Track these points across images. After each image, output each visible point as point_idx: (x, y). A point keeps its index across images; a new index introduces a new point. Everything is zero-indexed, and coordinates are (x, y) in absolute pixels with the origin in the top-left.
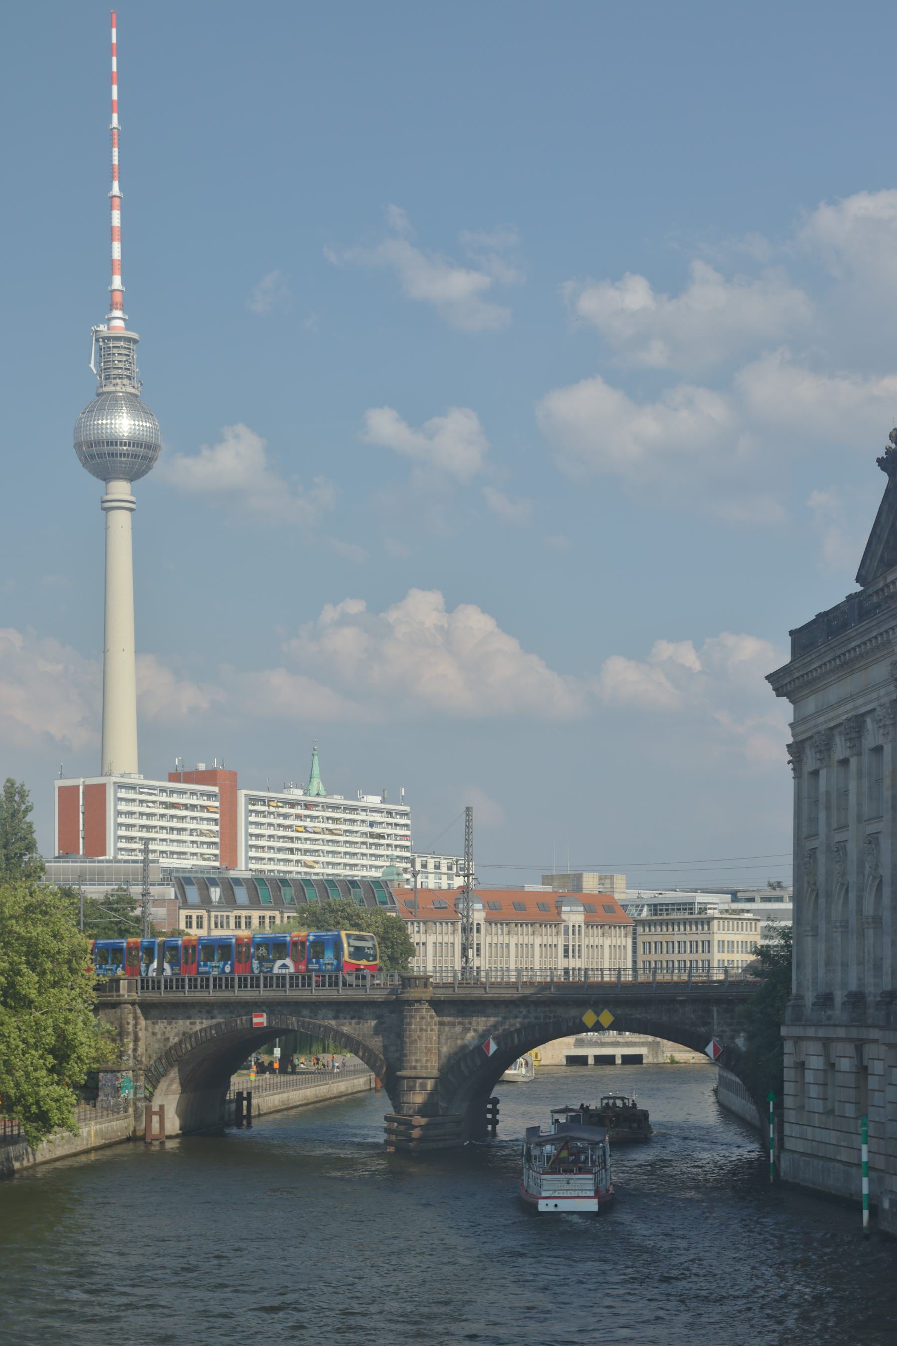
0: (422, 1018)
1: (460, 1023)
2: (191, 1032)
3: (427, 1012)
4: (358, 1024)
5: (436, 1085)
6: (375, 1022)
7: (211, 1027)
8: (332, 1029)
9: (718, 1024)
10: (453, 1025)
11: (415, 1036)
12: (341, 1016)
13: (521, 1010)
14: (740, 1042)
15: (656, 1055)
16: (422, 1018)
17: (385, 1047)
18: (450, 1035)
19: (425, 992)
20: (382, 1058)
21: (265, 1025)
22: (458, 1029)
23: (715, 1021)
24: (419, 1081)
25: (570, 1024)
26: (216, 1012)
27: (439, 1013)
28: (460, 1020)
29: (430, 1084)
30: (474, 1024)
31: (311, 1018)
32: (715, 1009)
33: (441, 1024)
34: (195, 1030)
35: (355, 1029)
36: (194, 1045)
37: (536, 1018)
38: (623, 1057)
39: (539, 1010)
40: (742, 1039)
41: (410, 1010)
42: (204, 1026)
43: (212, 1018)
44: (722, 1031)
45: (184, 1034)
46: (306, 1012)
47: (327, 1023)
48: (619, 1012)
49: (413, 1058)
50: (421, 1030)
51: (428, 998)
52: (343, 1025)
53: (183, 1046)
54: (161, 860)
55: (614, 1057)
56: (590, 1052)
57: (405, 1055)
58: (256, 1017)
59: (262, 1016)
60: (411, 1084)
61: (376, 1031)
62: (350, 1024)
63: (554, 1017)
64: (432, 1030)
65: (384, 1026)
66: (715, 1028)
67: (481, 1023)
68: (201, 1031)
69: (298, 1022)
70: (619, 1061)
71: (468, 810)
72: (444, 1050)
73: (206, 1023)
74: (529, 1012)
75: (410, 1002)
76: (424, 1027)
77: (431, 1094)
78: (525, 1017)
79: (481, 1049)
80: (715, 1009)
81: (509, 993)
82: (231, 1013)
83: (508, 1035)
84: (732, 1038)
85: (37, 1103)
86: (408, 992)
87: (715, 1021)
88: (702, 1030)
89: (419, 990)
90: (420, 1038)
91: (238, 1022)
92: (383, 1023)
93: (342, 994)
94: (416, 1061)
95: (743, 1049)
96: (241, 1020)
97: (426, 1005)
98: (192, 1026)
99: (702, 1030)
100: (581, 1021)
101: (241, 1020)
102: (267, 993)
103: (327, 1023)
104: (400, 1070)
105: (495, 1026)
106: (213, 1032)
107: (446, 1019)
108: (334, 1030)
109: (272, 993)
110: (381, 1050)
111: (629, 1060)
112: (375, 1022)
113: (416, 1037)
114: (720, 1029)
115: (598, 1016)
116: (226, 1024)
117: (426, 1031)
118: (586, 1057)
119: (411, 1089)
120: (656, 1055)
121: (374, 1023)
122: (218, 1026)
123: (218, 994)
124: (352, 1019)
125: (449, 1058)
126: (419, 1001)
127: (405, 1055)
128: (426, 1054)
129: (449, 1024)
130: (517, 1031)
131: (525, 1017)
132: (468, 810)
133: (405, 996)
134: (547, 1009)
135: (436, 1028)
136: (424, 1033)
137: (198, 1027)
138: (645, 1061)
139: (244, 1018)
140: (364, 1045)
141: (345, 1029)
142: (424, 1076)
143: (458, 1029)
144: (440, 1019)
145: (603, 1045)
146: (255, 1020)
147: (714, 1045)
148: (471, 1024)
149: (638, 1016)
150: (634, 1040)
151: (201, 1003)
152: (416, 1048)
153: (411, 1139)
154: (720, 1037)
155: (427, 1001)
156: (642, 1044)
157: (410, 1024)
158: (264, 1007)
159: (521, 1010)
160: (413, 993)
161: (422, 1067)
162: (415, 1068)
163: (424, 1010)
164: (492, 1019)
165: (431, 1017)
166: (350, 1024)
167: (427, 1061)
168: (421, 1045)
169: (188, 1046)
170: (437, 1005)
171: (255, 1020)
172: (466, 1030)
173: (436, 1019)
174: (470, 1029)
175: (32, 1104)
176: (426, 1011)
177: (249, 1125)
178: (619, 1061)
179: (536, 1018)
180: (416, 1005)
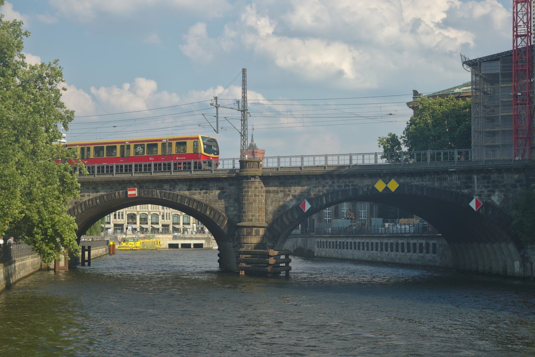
1: (281, 191)
2: (81, 202)
3: (259, 184)
4: (206, 193)
5: (265, 232)
6: (219, 191)
7: (96, 198)
8: (186, 197)
9: (478, 187)
10: (277, 192)
13: (327, 181)
16: (256, 188)
17: (226, 208)
18: (274, 199)
19: (257, 171)
20: (224, 215)
21: (137, 195)
22: (281, 195)
23: (476, 185)
24: (254, 229)
25: (365, 190)
27: (266, 184)
28: (282, 189)
29: (262, 231)
30: (292, 191)
31: (170, 190)
32: (475, 177)
33: (268, 192)
34: (84, 200)
35: (203, 197)
36: (84, 210)
37: (339, 186)
38: (182, 244)
39: (341, 181)
40: (497, 197)
41: (248, 183)
42: (91, 197)
43: (97, 192)
44: (481, 192)
46: (166, 186)
47: (182, 192)
48: (402, 181)
49: (250, 214)
50: (255, 195)
51: (260, 175)
52: (194, 194)
53: (76, 211)
55: (178, 245)
56: (180, 242)
57: (244, 212)
58: (130, 190)
59: (135, 190)
60: (249, 231)
61: (220, 197)
62: (200, 193)
64: (262, 196)
65: (225, 194)
66: (476, 190)
67: (297, 190)
68: (89, 200)
69: (161, 193)
70: (180, 246)
71: (244, 71)
72: (270, 209)
73: (93, 195)
74: (333, 183)
75: (247, 177)
78: (330, 186)
79: (298, 208)
80: (475, 177)
81: (320, 171)
83: (318, 197)
84: (489, 196)
86: (246, 171)
87: (476, 185)
88: (466, 191)
89: (254, 169)
90: (254, 201)
91: (117, 194)
92: (225, 192)
93: (195, 174)
94: (252, 216)
95: (498, 203)
96: (119, 193)
97: (258, 180)
98: (82, 198)
99: (466, 191)
100: (373, 187)
101: (119, 193)
102: (137, 175)
103: (182, 192)
104: (239, 222)
105: (308, 192)
106: (98, 201)
108: (188, 198)
111: (196, 246)
112: (219, 191)
113: (252, 201)
114: (480, 190)
115: (387, 184)
116: (107, 195)
117: (259, 196)
119: (249, 234)
121: (218, 192)
122: (101, 197)
123: (101, 176)
124: (201, 190)
125: (275, 213)
126: (254, 177)
127: (244, 212)
128: (259, 211)
129: (274, 192)
130: (324, 194)
131: (330, 186)
132: (244, 71)
133: (245, 173)
134: (347, 180)
135: (264, 194)
137: (86, 198)
139: (121, 191)
141: (197, 197)
142: (258, 225)
143: (281, 195)
144: (267, 189)
145: (185, 239)
148: (290, 191)
149: (416, 183)
151: (89, 182)
152: (252, 207)
153: (269, 265)
154: (480, 195)
155: (260, 176)
156: (203, 239)
157: (248, 191)
158: (135, 184)
160: (249, 171)
162: (251, 220)
164: (306, 188)
165: (262, 187)
166: (200, 193)
167: (259, 216)
168: (255, 205)
172: (286, 195)
173: (264, 189)
174: (289, 195)
176: (258, 184)
177: (89, 265)
178: (180, 246)
179: (339, 186)
180: (252, 179)
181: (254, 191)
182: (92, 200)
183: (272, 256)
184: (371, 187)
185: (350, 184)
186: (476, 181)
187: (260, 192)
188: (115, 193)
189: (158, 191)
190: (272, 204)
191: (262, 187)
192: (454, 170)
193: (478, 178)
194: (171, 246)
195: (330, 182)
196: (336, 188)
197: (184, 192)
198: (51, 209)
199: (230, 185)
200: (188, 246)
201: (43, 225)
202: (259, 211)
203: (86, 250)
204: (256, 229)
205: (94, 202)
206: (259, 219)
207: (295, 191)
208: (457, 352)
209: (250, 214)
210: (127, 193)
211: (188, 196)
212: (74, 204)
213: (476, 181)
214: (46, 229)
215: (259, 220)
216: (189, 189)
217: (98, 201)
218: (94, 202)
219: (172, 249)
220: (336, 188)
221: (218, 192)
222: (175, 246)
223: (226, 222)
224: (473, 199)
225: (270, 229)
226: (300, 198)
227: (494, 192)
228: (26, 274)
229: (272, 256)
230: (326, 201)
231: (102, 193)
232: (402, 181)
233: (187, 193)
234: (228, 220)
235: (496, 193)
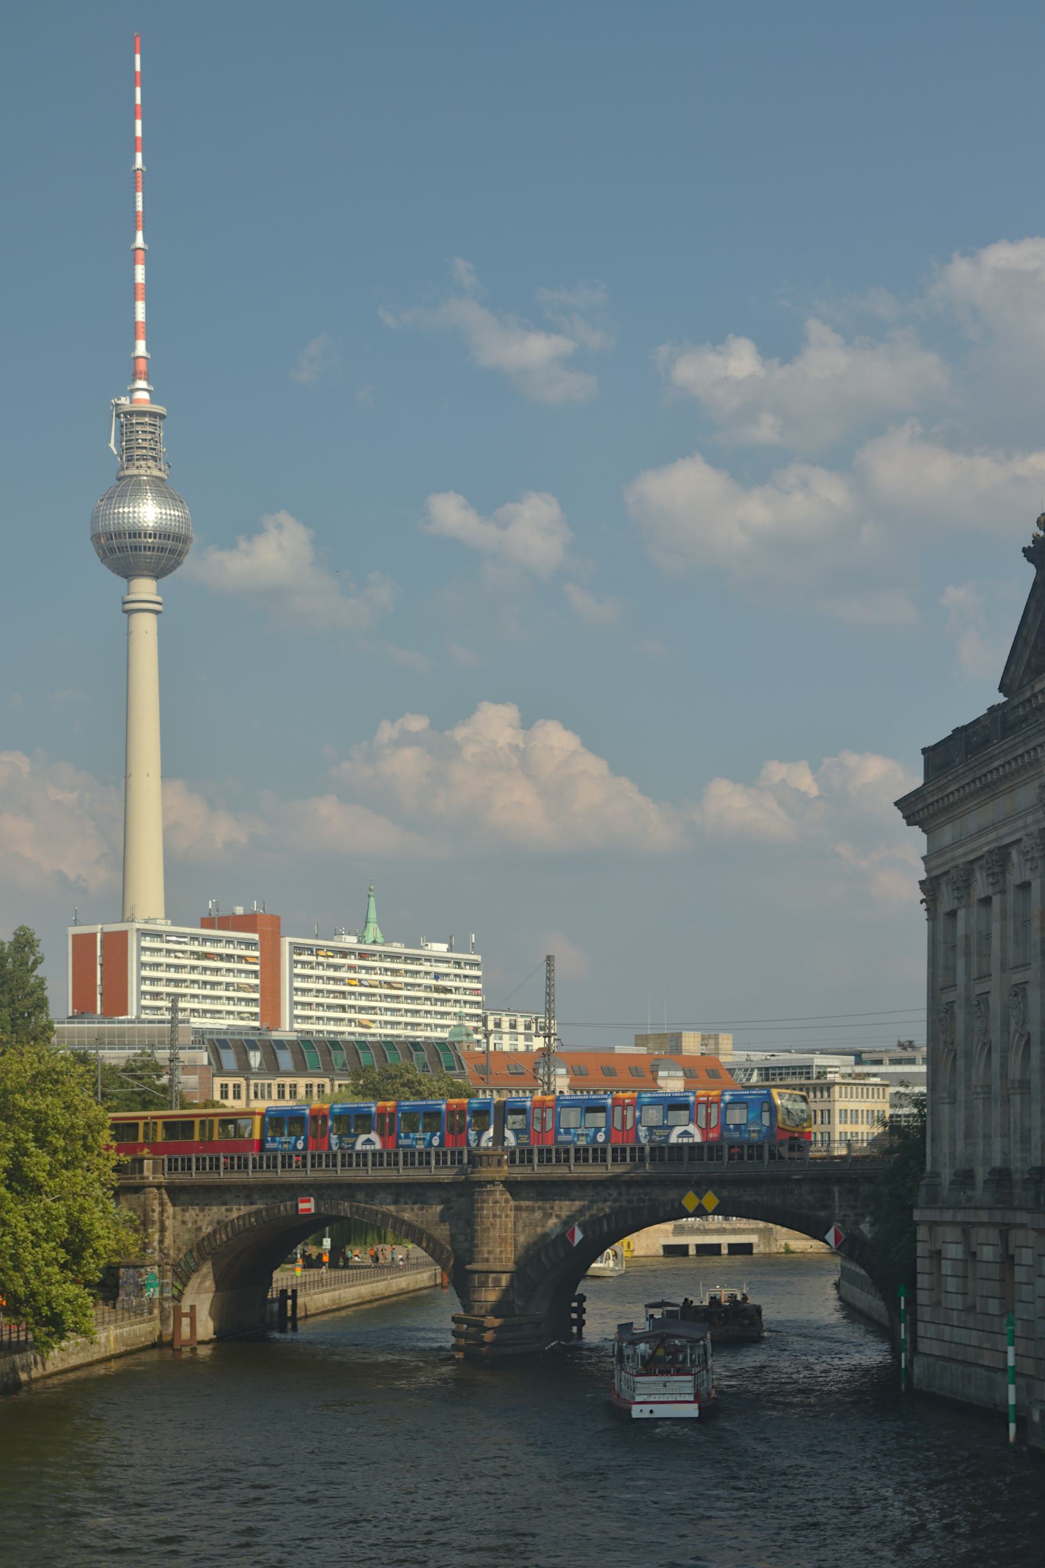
0: (496, 1202)
1: (539, 1208)
2: (227, 1220)
3: (502, 1194)
4: (422, 1209)
5: (512, 1280)
7: (250, 1215)
9: (841, 1206)
10: (532, 1210)
16: (496, 1202)
17: (453, 1237)
20: (450, 1249)
21: (313, 1211)
22: (538, 1215)
23: (837, 1204)
25: (669, 1208)
26: (256, 1196)
27: (515, 1196)
28: (540, 1204)
29: (505, 1279)
30: (556, 1208)
31: (366, 1203)
32: (836, 1189)
33: (518, 1209)
34: (231, 1218)
35: (417, 1216)
36: (230, 1235)
37: (628, 1201)
39: (632, 1192)
41: (481, 1193)
43: (252, 1204)
44: (844, 1215)
46: (360, 1196)
47: (384, 1208)
48: (725, 1193)
49: (485, 1249)
50: (495, 1216)
52: (404, 1211)
53: (218, 1236)
54: (192, 1020)
55: (719, 1246)
56: (692, 1241)
57: (476, 1246)
58: (302, 1201)
59: (309, 1201)
60: (483, 1279)
61: (443, 1218)
62: (412, 1210)
63: (649, 1200)
64: (507, 1216)
67: (565, 1208)
68: (238, 1218)
69: (351, 1207)
71: (549, 959)
72: (522, 1239)
73: (244, 1210)
74: (620, 1194)
75: (481, 1184)
76: (498, 1213)
78: (615, 1201)
79: (564, 1237)
80: (836, 1189)
83: (596, 1221)
84: (857, 1223)
86: (479, 1172)
87: (837, 1204)
90: (493, 1225)
91: (282, 1209)
94: (489, 1252)
96: (285, 1206)
97: (501, 1187)
98: (228, 1214)
99: (822, 1214)
100: (680, 1204)
101: (285, 1206)
104: (470, 1263)
106: (253, 1220)
107: (524, 1204)
108: (393, 1217)
110: (448, 1239)
113: (488, 1225)
114: (842, 1213)
115: (701, 1198)
116: (267, 1210)
117: (500, 1217)
119: (483, 1284)
122: (258, 1212)
123: (259, 1175)
124: (414, 1204)
125: (527, 1248)
126: (492, 1182)
127: (476, 1246)
128: (501, 1243)
129: (527, 1208)
130: (607, 1216)
131: (615, 1201)
132: (549, 959)
133: (476, 1177)
135: (512, 1214)
136: (498, 1220)
137: (235, 1215)
138: (755, 1251)
141: (407, 1216)
142: (498, 1269)
143: (538, 1215)
145: (706, 1232)
146: (301, 1206)
147: (836, 1231)
148: (552, 1208)
149: (747, 1198)
150: (742, 1226)
153: (483, 1344)
154: (843, 1222)
155: (502, 1182)
156: (752, 1231)
157: (482, 1209)
162: (487, 1260)
163: (498, 1193)
165: (507, 1201)
166: (412, 1210)
167: (501, 1252)
168: (494, 1233)
169: (223, 1236)
170: (513, 1187)
171: (301, 1206)
172: (547, 1216)
173: (512, 1203)
174: (551, 1215)
176: (500, 1194)
177: (295, 1328)
179: (628, 1201)
180: (489, 1187)
181: (492, 1207)
182: (243, 1216)
183: (489, 1329)
184: (676, 1205)
186: (837, 1197)
187: (502, 1209)
189: (346, 1204)
190: (524, 1231)
191: (507, 1201)
193: (840, 1192)
194: (670, 1250)
195: (615, 1194)
196: (624, 1203)
199: (460, 1196)
200: (713, 1250)
201: (35, 1300)
202: (501, 1243)
203: (289, 1298)
204: (494, 1275)
205: (247, 1221)
207: (561, 1208)
208: (200, 1488)
209: (485, 1249)
210: (297, 1205)
211: (395, 1213)
212: (215, 1225)
213: (837, 1197)
214: (40, 1308)
215: (501, 1260)
216: (395, 1202)
217: (253, 1220)
218: (247, 1221)
219: (669, 1259)
220: (624, 1203)
221: (439, 1208)
222: (680, 1251)
225: (518, 1274)
227: (863, 1216)
228: (90, 1359)
229: (489, 1329)
230: (608, 1227)
232: (725, 1193)
233: (392, 1208)
234: (456, 1259)
235: (867, 1219)
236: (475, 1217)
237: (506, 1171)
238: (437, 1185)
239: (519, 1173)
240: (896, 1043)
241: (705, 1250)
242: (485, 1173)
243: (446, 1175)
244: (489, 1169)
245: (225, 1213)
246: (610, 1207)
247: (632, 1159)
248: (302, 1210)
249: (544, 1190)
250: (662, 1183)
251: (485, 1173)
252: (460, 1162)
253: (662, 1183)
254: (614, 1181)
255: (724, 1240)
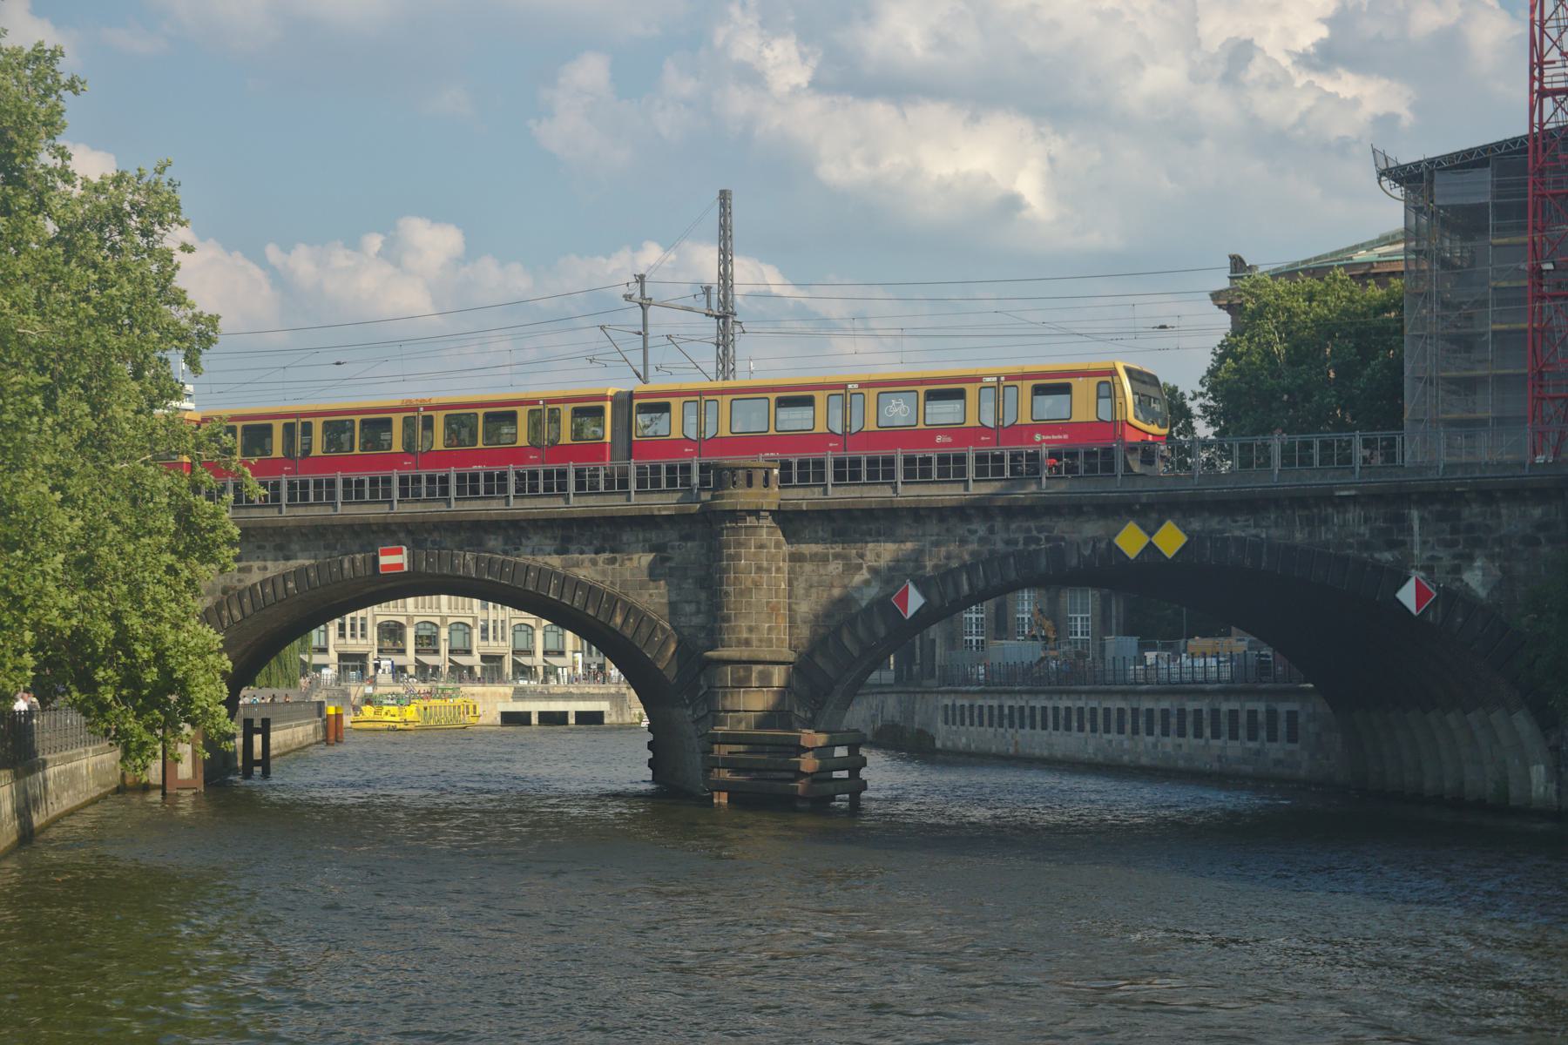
0: (762, 546)
1: (837, 556)
2: (241, 586)
3: (769, 534)
4: (612, 561)
5: (789, 677)
6: (651, 556)
7: (285, 577)
8: (553, 573)
9: (1424, 543)
10: (824, 559)
11: (747, 580)
12: (573, 548)
13: (973, 527)
14: (1475, 579)
15: (621, 712)
16: (762, 546)
17: (673, 607)
18: (815, 578)
21: (406, 568)
22: (835, 567)
23: (1417, 538)
24: (756, 668)
25: (1087, 552)
26: (295, 547)
27: (790, 536)
28: (838, 548)
29: (778, 676)
30: (869, 556)
31: (506, 553)
32: (1415, 514)
33: (795, 558)
34: (249, 583)
35: (604, 573)
36: (248, 610)
37: (1007, 542)
39: (1013, 526)
40: (1479, 573)
41: (736, 530)
42: (269, 574)
43: (287, 558)
44: (1433, 558)
45: (225, 591)
46: (494, 542)
47: (541, 560)
48: (1196, 525)
49: (743, 624)
50: (759, 569)
52: (577, 564)
53: (225, 613)
55: (565, 714)
56: (535, 707)
57: (727, 619)
58: (385, 553)
59: (400, 552)
60: (742, 673)
61: (654, 573)
63: (1048, 539)
64: (778, 570)
66: (1416, 552)
67: (883, 552)
68: (263, 583)
69: (477, 560)
70: (535, 720)
71: (724, 196)
72: (804, 608)
73: (274, 568)
74: (991, 531)
75: (735, 515)
76: (765, 564)
77: (786, 689)
78: (982, 540)
79: (886, 607)
80: (1415, 514)
82: (327, 547)
83: (946, 575)
84: (1457, 570)
85: (160, 656)
86: (731, 496)
87: (1417, 538)
88: (1387, 556)
90: (757, 585)
91: (346, 565)
93: (578, 504)
94: (750, 629)
95: (1482, 593)
96: (353, 562)
97: (768, 522)
98: (242, 576)
99: (1387, 556)
100: (1111, 544)
101: (353, 562)
103: (541, 560)
106: (291, 585)
107: (807, 549)
108: (558, 575)
109: (418, 508)
110: (666, 611)
111: (585, 718)
112: (651, 556)
113: (749, 583)
115: (1151, 534)
117: (769, 570)
118: (529, 714)
119: (742, 683)
120: (621, 712)
122: (301, 573)
123: (300, 511)
126: (756, 513)
127: (727, 619)
128: (770, 615)
129: (814, 557)
130: (964, 566)
131: (982, 540)
132: (724, 196)
133: (727, 503)
134: (1032, 525)
135: (785, 566)
136: (765, 576)
137: (255, 577)
138: (606, 721)
140: (625, 603)
141: (585, 573)
142: (768, 658)
143: (835, 567)
144: (794, 548)
145: (551, 697)
146: (384, 560)
147: (1417, 582)
148: (862, 556)
149: (1237, 533)
150: (592, 691)
152: (749, 604)
154: (1429, 570)
156: (602, 697)
157: (737, 557)
158: (402, 535)
159: (973, 527)
161: (760, 640)
162: (747, 643)
163: (765, 531)
164: (909, 546)
165: (778, 545)
166: (594, 563)
167: (770, 629)
168: (760, 598)
169: (236, 613)
170: (790, 521)
171: (384, 560)
173: (786, 548)
174: (860, 567)
175: (147, 663)
176: (767, 533)
177: (266, 773)
178: (535, 720)
180: (751, 521)
182: (273, 580)
183: (808, 750)
185: (1042, 536)
186: (1416, 528)
187: (772, 558)
188: (341, 562)
190: (807, 595)
192: (1353, 492)
193: (1422, 519)
194: (509, 718)
195: (981, 529)
196: (1000, 546)
197: (548, 559)
198: (149, 606)
202: (770, 615)
204: (760, 667)
206: (770, 640)
207: (878, 555)
209: (743, 624)
210: (376, 560)
212: (218, 594)
213: (1416, 528)
220: (1000, 546)
223: (672, 649)
224: (1407, 579)
225: (802, 669)
226: (891, 577)
227: (1470, 558)
229: (808, 750)
231: (303, 561)
232: (1196, 525)
233: (555, 561)
234: (679, 643)
235: (1478, 563)
236: (725, 570)
237: (773, 497)
238: (646, 521)
239: (803, 497)
240: (1074, 389)
241: (548, 718)
242: (741, 497)
243: (663, 503)
244: (750, 491)
245: (237, 575)
246: (972, 554)
247: (1013, 470)
248: (386, 567)
249: (846, 525)
250: (1076, 509)
251: (741, 497)
252: (687, 482)
253: (1076, 509)
254: (962, 512)
255: (572, 707)
